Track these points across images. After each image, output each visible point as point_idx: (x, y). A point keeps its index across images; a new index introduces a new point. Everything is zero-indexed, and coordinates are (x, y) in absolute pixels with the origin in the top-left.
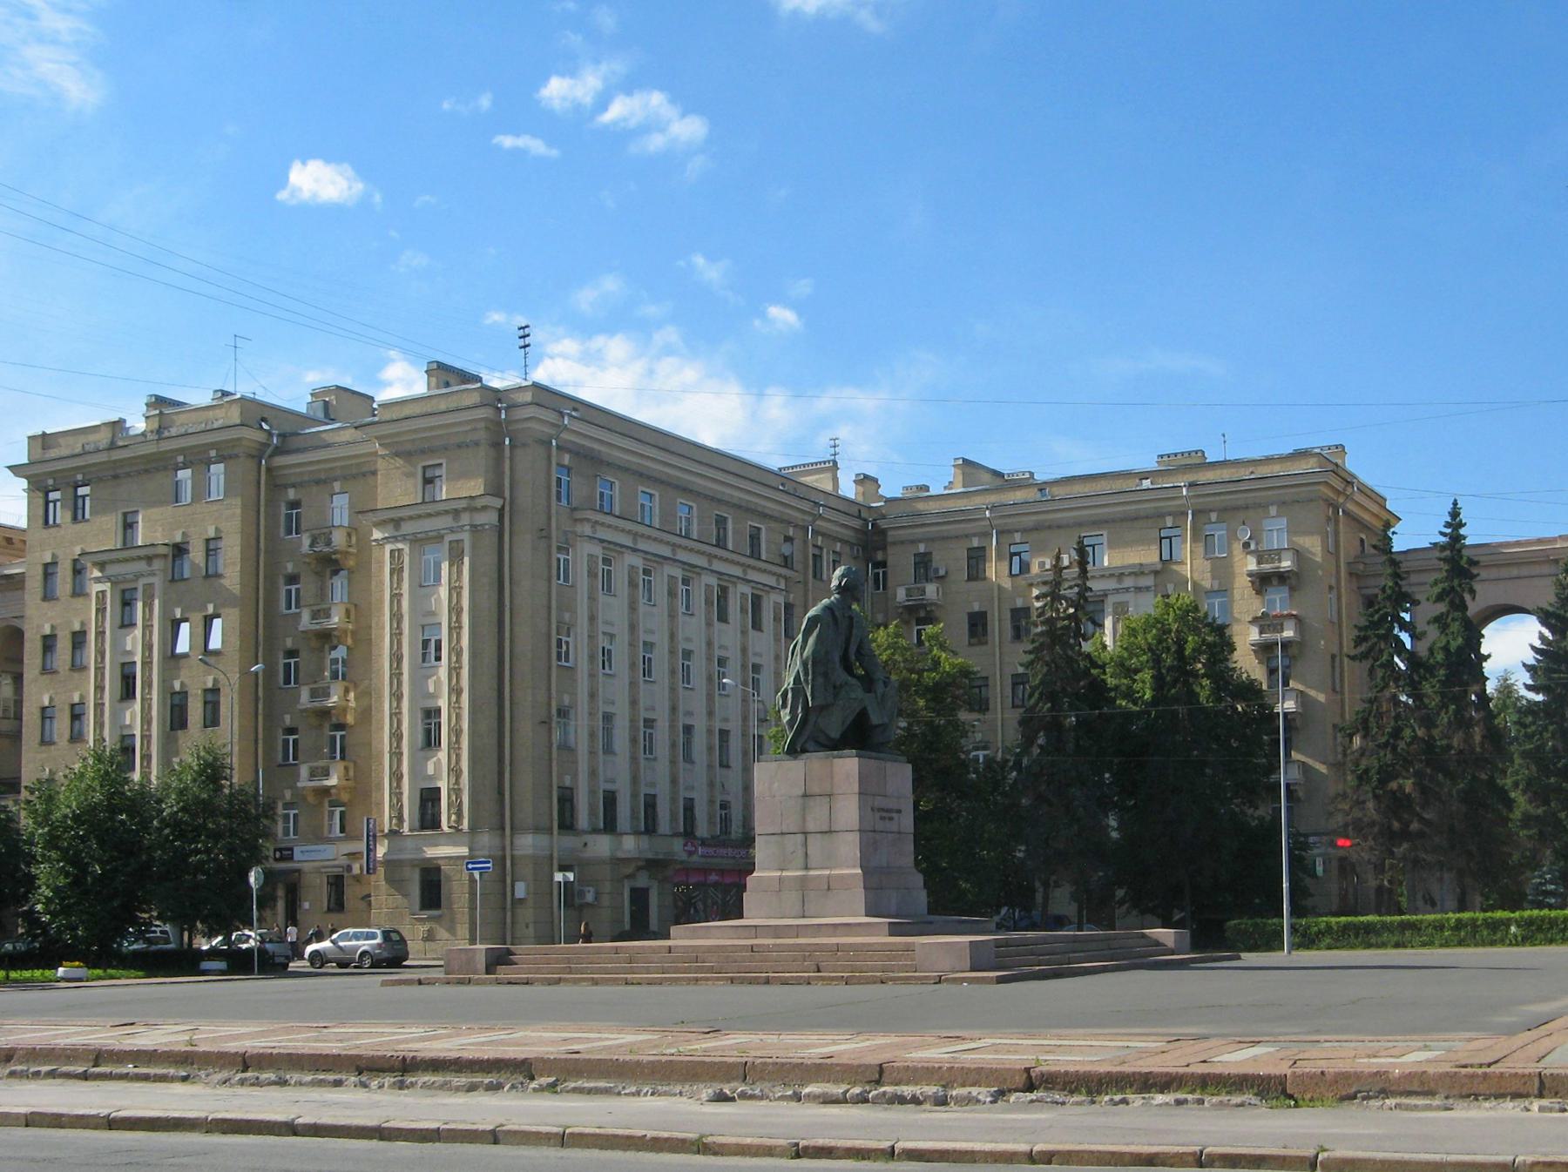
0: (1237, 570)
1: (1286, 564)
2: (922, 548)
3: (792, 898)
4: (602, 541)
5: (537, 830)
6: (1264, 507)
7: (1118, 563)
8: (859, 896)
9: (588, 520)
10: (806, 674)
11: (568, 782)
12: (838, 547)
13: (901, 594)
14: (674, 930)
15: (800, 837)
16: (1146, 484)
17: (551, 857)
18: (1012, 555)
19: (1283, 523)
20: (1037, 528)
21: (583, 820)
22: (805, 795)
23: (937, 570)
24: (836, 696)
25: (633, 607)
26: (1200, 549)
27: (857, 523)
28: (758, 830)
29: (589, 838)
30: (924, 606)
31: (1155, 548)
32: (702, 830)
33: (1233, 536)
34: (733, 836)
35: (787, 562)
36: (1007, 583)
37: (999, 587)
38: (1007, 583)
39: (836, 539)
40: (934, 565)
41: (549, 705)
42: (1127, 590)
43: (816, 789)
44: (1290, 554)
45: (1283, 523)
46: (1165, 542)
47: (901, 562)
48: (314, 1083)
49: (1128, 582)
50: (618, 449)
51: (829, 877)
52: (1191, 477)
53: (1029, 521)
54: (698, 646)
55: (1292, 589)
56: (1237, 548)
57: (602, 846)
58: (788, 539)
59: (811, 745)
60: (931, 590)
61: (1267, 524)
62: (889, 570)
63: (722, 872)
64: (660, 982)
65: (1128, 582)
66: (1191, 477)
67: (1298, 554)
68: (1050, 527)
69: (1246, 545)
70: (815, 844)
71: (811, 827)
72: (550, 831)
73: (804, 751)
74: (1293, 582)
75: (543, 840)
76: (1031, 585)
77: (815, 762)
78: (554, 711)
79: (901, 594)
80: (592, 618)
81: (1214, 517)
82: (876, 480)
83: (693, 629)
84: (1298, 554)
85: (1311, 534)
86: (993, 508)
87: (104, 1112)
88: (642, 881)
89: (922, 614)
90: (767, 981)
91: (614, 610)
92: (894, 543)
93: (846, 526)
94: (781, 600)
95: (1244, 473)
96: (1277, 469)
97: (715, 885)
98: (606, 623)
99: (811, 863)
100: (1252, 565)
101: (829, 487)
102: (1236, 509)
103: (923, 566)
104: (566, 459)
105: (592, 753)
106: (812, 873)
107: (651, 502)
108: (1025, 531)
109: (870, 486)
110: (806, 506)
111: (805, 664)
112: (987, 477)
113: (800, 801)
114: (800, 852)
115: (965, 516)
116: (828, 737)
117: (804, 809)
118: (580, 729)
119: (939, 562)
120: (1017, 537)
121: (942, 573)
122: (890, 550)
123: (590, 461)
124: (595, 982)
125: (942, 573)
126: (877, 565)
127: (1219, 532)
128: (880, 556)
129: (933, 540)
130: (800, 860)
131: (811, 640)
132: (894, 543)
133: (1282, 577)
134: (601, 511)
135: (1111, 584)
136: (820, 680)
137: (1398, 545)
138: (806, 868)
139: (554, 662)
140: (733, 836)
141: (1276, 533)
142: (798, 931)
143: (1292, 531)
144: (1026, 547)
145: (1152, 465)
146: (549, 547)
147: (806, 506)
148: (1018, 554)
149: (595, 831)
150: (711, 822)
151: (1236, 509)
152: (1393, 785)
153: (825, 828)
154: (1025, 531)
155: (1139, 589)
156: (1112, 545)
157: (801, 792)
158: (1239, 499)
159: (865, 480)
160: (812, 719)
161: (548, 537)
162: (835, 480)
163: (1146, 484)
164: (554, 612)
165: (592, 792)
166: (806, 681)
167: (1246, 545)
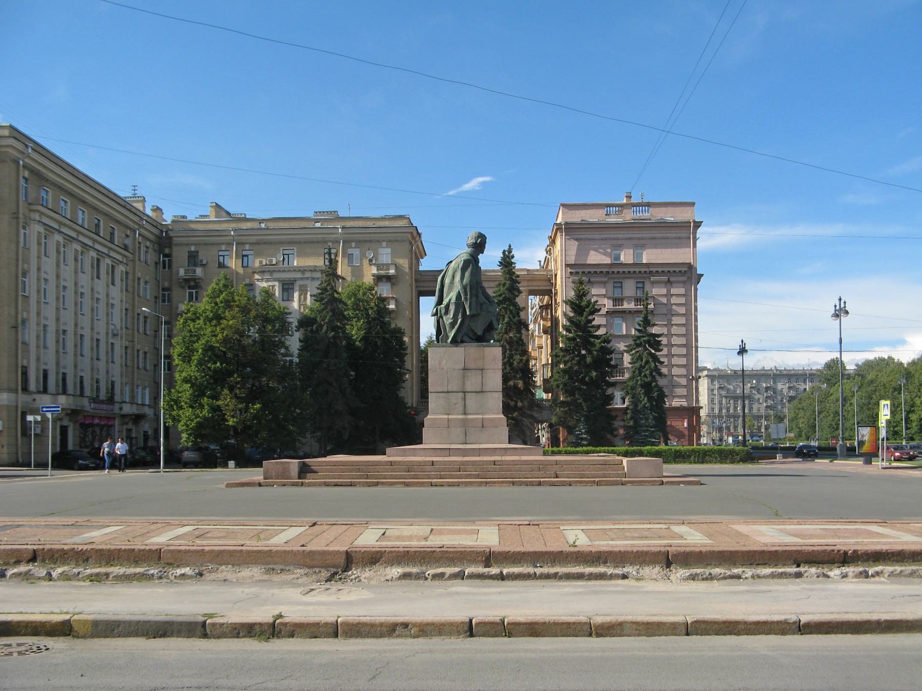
0: (365, 273)
1: (392, 271)
2: (193, 248)
3: (458, 432)
4: (45, 224)
5: (10, 390)
6: (379, 242)
7: (302, 264)
8: (505, 431)
9: (38, 211)
10: (466, 294)
11: (25, 364)
12: (148, 244)
13: (182, 272)
14: (388, 450)
15: (461, 395)
16: (318, 225)
17: (17, 406)
18: (244, 256)
19: (389, 250)
20: (257, 243)
21: (32, 386)
22: (464, 369)
23: (201, 261)
24: (481, 308)
25: (58, 266)
26: (346, 261)
27: (156, 232)
28: (430, 389)
29: (37, 396)
30: (194, 280)
31: (322, 258)
32: (88, 392)
33: (363, 256)
34: (101, 398)
35: (126, 248)
36: (241, 271)
37: (237, 273)
38: (241, 271)
39: (149, 240)
40: (200, 258)
41: (17, 317)
42: (307, 278)
43: (471, 365)
44: (393, 266)
45: (389, 250)
46: (286, 257)
47: (180, 256)
48: (772, 576)
49: (308, 275)
50: (52, 173)
51: (483, 419)
52: (343, 224)
53: (253, 239)
54: (87, 291)
55: (393, 284)
56: (366, 262)
57: (62, 399)
58: (127, 236)
59: (466, 338)
60: (199, 271)
61: (381, 251)
62: (174, 259)
63: (100, 418)
64: (458, 484)
65: (308, 275)
66: (343, 224)
67: (397, 267)
68: (265, 243)
69: (371, 260)
70: (471, 400)
71: (469, 388)
72: (16, 391)
73: (462, 342)
74: (393, 281)
75: (13, 396)
76: (254, 272)
77: (471, 350)
78: (20, 321)
79: (182, 272)
80: (39, 269)
81: (353, 245)
82: (161, 210)
83: (85, 280)
84: (397, 267)
85: (402, 258)
86: (235, 230)
87: (793, 618)
88: (66, 422)
89: (192, 283)
90: (540, 484)
91: (49, 265)
92: (177, 245)
93: (152, 233)
94: (124, 269)
95: (370, 224)
96: (387, 224)
97: (97, 425)
98: (45, 272)
99: (469, 410)
100: (374, 270)
101: (141, 209)
102: (365, 241)
103: (193, 259)
104: (26, 174)
105: (38, 347)
106: (470, 417)
107: (67, 206)
108: (251, 244)
109: (159, 212)
110: (136, 219)
111: (465, 288)
112: (224, 214)
113: (461, 372)
114: (461, 403)
115: (220, 233)
116: (475, 334)
117: (464, 377)
118: (31, 335)
119: (203, 256)
120: (247, 247)
121: (204, 262)
122: (174, 248)
123: (38, 176)
124: (407, 485)
125: (204, 262)
126: (165, 256)
127: (356, 252)
128: (167, 251)
129: (199, 244)
130: (461, 409)
131: (467, 274)
132: (177, 245)
133: (388, 278)
134: (42, 205)
135: (299, 275)
136: (474, 299)
137: (421, 268)
138: (465, 414)
139: (20, 293)
140: (101, 398)
141: (385, 255)
142: (465, 452)
143: (394, 254)
144: (252, 252)
145: (310, 215)
146: (18, 224)
147: (136, 219)
148: (247, 256)
149: (39, 392)
150: (92, 390)
151: (365, 241)
152: (511, 383)
153: (478, 389)
154: (251, 244)
155: (313, 279)
156: (300, 255)
157: (462, 366)
158: (367, 237)
159: (157, 209)
160: (467, 322)
161: (18, 218)
162: (144, 207)
163: (318, 225)
164: (20, 263)
165: (38, 370)
166: (466, 299)
167: (371, 260)
